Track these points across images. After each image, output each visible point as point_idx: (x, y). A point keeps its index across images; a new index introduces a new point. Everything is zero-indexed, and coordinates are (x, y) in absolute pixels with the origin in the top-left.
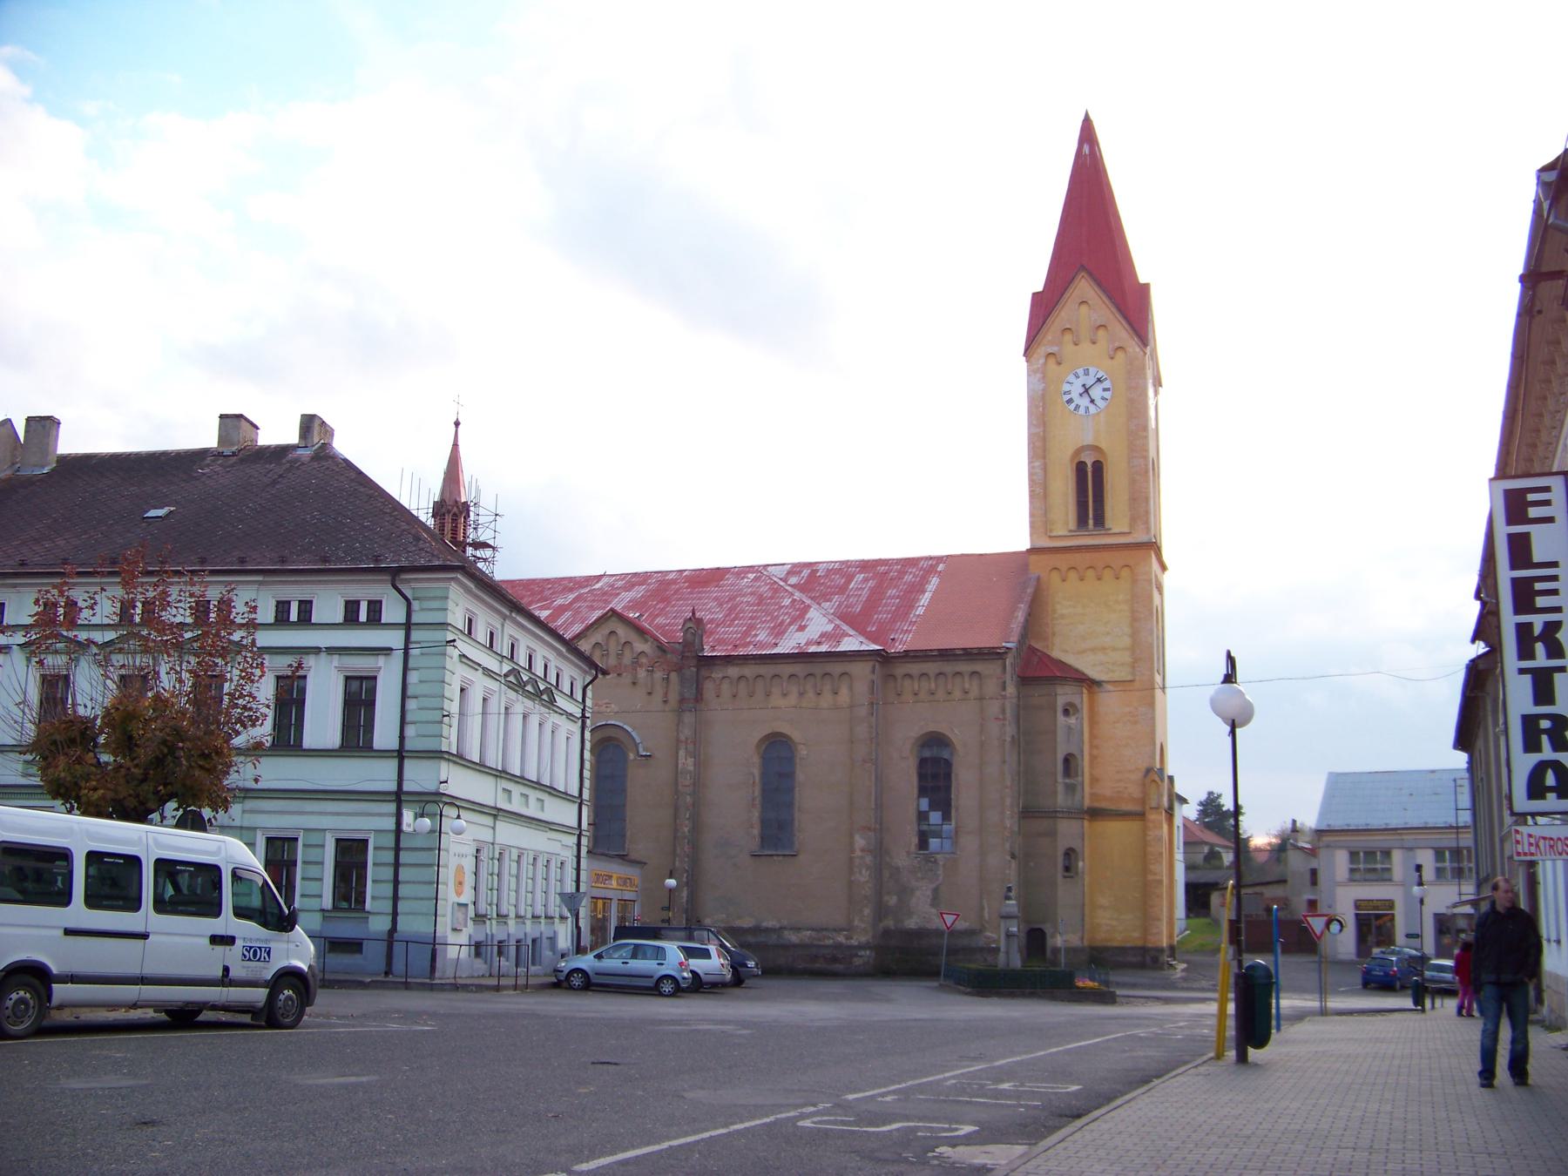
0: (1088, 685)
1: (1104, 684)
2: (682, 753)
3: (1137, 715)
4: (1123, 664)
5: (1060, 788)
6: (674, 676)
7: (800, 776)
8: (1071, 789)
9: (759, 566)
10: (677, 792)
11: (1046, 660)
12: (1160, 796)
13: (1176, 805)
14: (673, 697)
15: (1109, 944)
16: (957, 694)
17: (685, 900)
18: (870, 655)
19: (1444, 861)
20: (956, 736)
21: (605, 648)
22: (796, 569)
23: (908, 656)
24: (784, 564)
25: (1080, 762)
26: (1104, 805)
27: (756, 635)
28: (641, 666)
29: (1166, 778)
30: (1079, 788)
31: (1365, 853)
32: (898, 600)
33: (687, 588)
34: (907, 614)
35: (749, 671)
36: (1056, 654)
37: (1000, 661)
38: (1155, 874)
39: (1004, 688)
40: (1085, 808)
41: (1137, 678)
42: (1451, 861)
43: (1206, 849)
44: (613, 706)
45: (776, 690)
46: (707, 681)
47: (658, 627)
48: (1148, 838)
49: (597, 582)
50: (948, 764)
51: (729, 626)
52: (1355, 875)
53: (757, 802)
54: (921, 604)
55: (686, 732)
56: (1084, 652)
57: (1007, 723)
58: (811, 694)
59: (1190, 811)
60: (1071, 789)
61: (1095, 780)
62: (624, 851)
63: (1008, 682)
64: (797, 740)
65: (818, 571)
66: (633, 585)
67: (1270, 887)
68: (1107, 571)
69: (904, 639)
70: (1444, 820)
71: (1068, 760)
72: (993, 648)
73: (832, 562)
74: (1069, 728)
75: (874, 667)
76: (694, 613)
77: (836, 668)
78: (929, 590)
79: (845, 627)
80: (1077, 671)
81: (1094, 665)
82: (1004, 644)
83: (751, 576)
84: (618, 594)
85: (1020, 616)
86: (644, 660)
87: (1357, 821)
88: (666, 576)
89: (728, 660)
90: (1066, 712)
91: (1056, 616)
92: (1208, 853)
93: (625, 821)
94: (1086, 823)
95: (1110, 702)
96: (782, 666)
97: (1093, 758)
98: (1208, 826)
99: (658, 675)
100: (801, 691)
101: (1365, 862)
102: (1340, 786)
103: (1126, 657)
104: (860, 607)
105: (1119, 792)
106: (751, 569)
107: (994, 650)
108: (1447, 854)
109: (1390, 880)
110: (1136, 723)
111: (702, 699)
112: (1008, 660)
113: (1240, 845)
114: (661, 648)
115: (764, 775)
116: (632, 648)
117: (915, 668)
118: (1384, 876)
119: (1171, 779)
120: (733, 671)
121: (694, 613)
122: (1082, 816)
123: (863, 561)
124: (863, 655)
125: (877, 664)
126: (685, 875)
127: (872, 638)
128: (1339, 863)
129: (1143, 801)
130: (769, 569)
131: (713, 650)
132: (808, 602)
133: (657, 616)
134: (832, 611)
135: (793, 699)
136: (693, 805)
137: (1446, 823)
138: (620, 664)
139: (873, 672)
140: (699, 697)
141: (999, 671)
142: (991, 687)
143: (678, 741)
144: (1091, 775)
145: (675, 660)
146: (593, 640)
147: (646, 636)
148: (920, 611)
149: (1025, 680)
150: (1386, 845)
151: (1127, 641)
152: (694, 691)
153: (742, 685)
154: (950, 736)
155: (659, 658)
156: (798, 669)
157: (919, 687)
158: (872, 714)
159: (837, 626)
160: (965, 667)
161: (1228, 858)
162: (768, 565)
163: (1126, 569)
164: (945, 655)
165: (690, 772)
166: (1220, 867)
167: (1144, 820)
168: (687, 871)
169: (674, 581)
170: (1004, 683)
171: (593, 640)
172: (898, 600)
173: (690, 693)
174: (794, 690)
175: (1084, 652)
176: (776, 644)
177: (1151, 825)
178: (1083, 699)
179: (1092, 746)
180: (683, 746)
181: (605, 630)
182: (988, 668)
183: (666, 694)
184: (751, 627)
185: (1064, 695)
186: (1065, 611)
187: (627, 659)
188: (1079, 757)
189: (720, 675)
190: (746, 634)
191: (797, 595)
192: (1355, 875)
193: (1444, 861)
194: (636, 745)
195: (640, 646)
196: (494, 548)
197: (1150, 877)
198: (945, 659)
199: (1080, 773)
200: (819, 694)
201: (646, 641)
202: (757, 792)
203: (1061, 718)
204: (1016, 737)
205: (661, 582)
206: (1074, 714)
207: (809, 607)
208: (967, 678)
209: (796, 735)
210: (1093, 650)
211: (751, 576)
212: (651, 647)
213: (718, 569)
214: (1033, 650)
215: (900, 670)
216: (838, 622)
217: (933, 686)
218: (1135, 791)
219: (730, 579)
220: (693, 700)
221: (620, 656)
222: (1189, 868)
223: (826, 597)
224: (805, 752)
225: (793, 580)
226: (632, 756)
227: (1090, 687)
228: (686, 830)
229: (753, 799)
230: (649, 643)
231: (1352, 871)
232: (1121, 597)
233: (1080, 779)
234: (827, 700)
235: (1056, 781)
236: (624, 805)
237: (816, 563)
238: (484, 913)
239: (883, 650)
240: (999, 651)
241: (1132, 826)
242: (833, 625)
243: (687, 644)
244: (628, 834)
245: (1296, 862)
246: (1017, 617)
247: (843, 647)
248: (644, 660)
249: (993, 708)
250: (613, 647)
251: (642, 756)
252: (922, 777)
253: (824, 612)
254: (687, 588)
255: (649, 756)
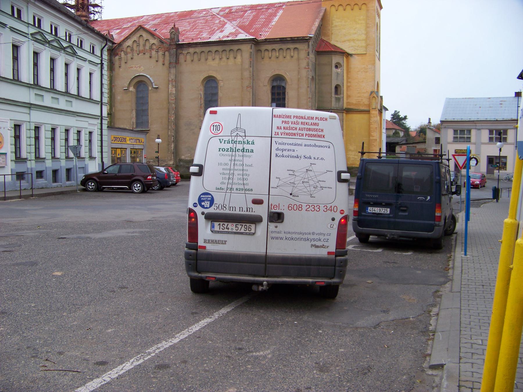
0: (346, 55)
1: (353, 55)
2: (170, 86)
3: (367, 69)
4: (362, 47)
5: (333, 99)
6: (167, 53)
7: (220, 94)
8: (338, 100)
9: (208, 9)
10: (169, 103)
11: (328, 44)
12: (377, 103)
13: (383, 111)
14: (167, 63)
15: (353, 166)
16: (288, 57)
17: (173, 148)
18: (249, 41)
19: (493, 134)
20: (287, 76)
21: (138, 43)
22: (223, 9)
23: (267, 41)
24: (218, 8)
25: (342, 88)
26: (352, 107)
27: (202, 35)
28: (153, 49)
29: (379, 97)
30: (342, 100)
31: (460, 131)
32: (264, 20)
33: (178, 18)
34: (268, 25)
35: (198, 50)
36: (333, 42)
37: (307, 43)
38: (374, 137)
39: (308, 55)
40: (344, 108)
41: (368, 52)
42: (496, 135)
43: (394, 131)
44: (142, 67)
45: (210, 58)
46: (181, 54)
47: (162, 34)
48: (371, 121)
49: (142, 19)
50: (284, 88)
51: (192, 32)
52: (456, 140)
53: (203, 106)
54: (274, 21)
55: (172, 77)
56: (345, 41)
57: (310, 70)
58: (224, 59)
59: (388, 116)
60: (338, 100)
61: (348, 96)
62: (148, 128)
63: (310, 52)
64: (218, 79)
65: (232, 10)
66: (156, 19)
67: (419, 144)
68: (356, 6)
69: (265, 34)
70: (494, 117)
71: (337, 87)
72: (304, 37)
73: (239, 6)
74: (338, 73)
75: (252, 46)
76: (174, 26)
77: (235, 47)
78: (278, 15)
79: (240, 30)
80: (341, 49)
81: (349, 47)
82: (308, 35)
83: (204, 13)
84: (149, 22)
85: (317, 24)
86: (154, 47)
87: (458, 118)
88: (170, 14)
89: (189, 45)
90: (336, 67)
91: (333, 26)
92: (395, 132)
93: (148, 116)
94: (344, 114)
95: (355, 62)
96: (212, 47)
97: (348, 87)
98: (394, 123)
99: (161, 53)
100: (220, 58)
101: (460, 134)
102: (450, 103)
103: (363, 44)
104: (248, 22)
105: (359, 101)
106: (205, 10)
107: (304, 38)
108: (494, 132)
109: (470, 142)
110: (367, 72)
111: (179, 63)
112: (310, 42)
113: (406, 130)
114: (161, 41)
115: (205, 94)
116: (149, 42)
117: (270, 47)
118: (468, 140)
119: (381, 97)
120: (192, 50)
121: (174, 26)
122: (343, 111)
123: (252, 5)
124: (247, 41)
125: (253, 45)
126: (173, 138)
127: (251, 34)
128: (449, 135)
129: (369, 105)
130: (212, 10)
131: (183, 41)
132: (226, 21)
133: (163, 30)
134: (236, 24)
135: (217, 60)
136: (176, 108)
137: (494, 119)
138: (145, 49)
139: (251, 48)
140: (177, 62)
141: (306, 47)
142: (303, 54)
143: (169, 81)
144: (347, 94)
145: (167, 46)
146: (133, 40)
147: (155, 36)
148: (273, 23)
149: (319, 53)
150: (469, 127)
151: (363, 37)
152: (175, 59)
153: (196, 56)
154: (284, 76)
155: (161, 45)
156: (220, 48)
157: (271, 55)
158: (251, 67)
159: (237, 30)
160: (291, 46)
161: (402, 134)
162: (212, 8)
163: (364, 5)
164: (283, 40)
165: (174, 94)
166: (399, 137)
167: (369, 114)
168: (173, 136)
169: (173, 16)
170: (309, 52)
171: (133, 40)
172: (264, 20)
173: (173, 60)
174: (217, 57)
175: (345, 41)
176: (210, 38)
177: (372, 116)
178: (343, 60)
179: (347, 82)
180: (171, 83)
181: (138, 35)
182: (302, 47)
183: (164, 61)
184: (201, 32)
185: (335, 59)
186: (337, 24)
187: (147, 47)
188: (342, 86)
189: (186, 52)
190: (198, 34)
191: (222, 19)
192: (456, 140)
193: (493, 134)
194: (152, 83)
195: (152, 41)
196: (101, 7)
197: (371, 138)
198: (283, 42)
199: (342, 92)
200: (228, 59)
201: (155, 38)
202: (203, 102)
203: (334, 69)
204: (314, 77)
205: (167, 17)
206: (340, 68)
207: (226, 23)
208: (292, 51)
209: (218, 77)
210: (349, 41)
211: (204, 13)
212: (157, 41)
213: (191, 11)
214: (323, 41)
215: (263, 47)
216: (237, 28)
217: (277, 54)
218: (366, 102)
219: (196, 15)
220: (175, 63)
221: (144, 45)
222: (388, 137)
223: (234, 19)
224: (222, 84)
225: (222, 13)
226: (150, 88)
227: (347, 56)
228: (173, 118)
229: (201, 105)
230: (156, 39)
231: (454, 138)
232: (362, 17)
233: (342, 95)
234: (231, 61)
235: (332, 96)
236: (148, 109)
237: (232, 7)
238: (25, 157)
239: (255, 38)
240: (306, 38)
241: (365, 116)
242: (235, 29)
243: (171, 39)
244: (150, 122)
245: (430, 136)
246: (315, 24)
247: (238, 38)
248: (154, 47)
249: (304, 64)
250: (142, 42)
251: (154, 88)
252: (273, 94)
253: (232, 25)
254: (178, 18)
255: (157, 88)
